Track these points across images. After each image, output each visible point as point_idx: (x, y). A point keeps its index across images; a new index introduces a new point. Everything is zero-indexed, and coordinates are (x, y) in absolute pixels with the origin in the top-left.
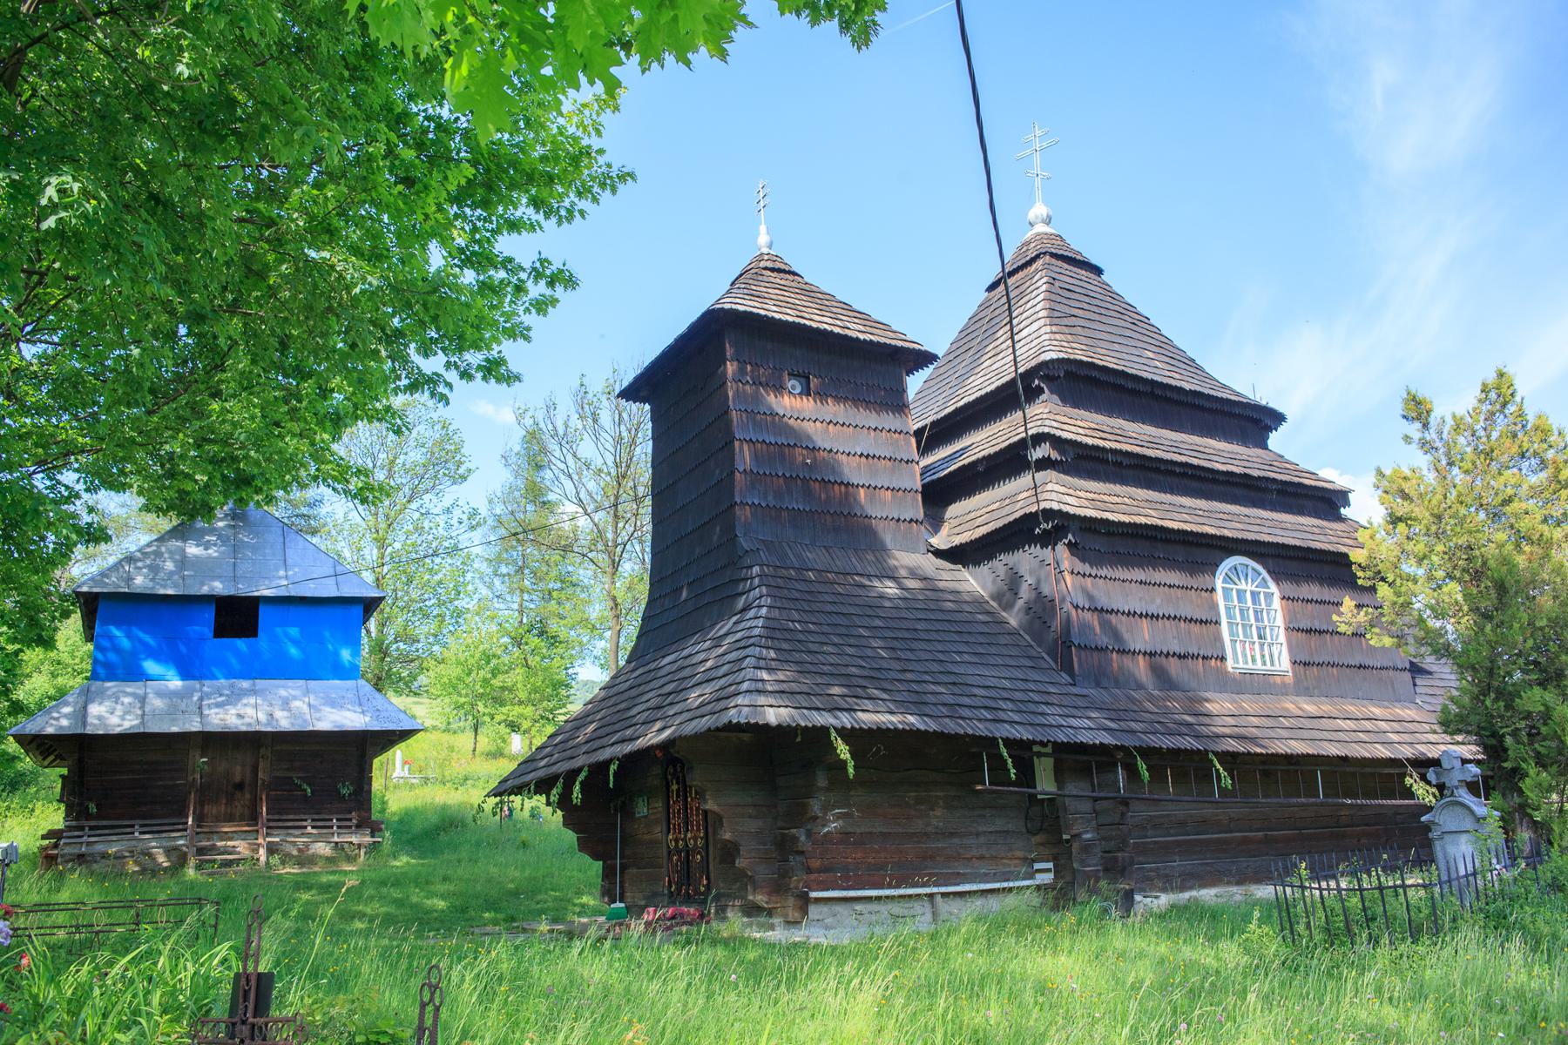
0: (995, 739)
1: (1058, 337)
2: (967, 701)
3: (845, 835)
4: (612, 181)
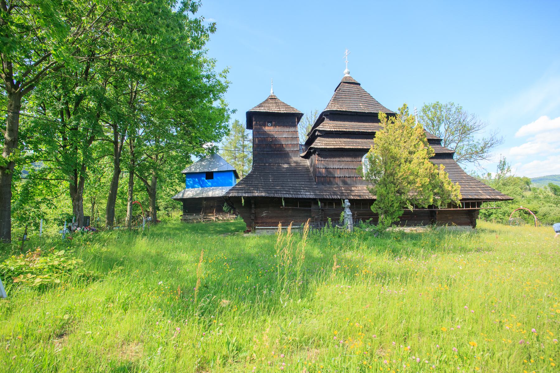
3: (267, 217)
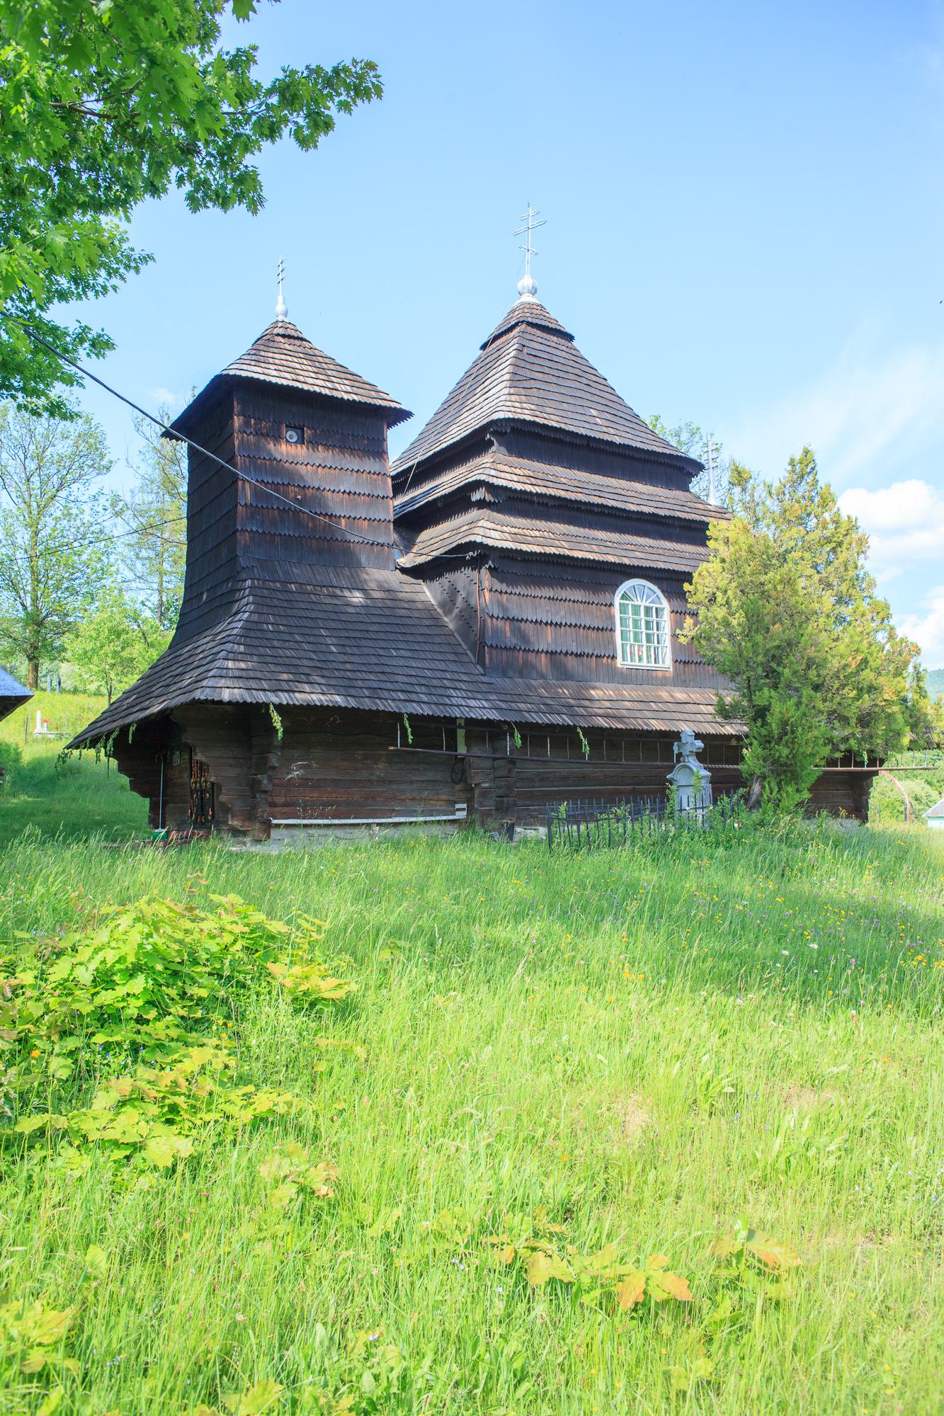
0: (401, 715)
1: (513, 398)
2: (389, 686)
3: (304, 782)
4: (135, 263)
